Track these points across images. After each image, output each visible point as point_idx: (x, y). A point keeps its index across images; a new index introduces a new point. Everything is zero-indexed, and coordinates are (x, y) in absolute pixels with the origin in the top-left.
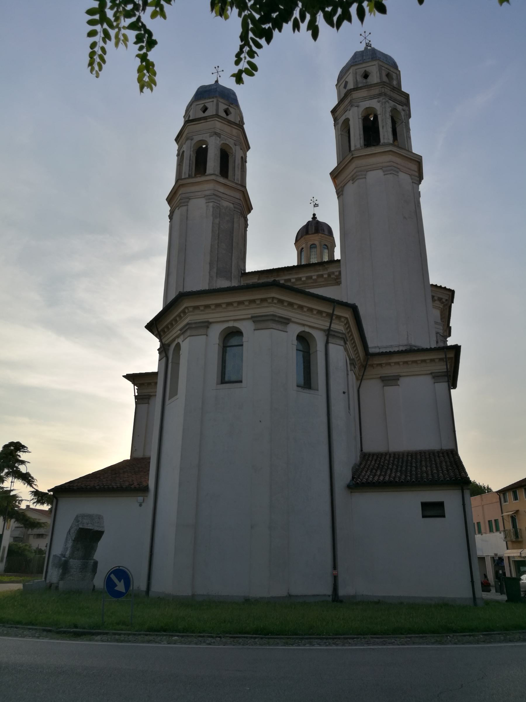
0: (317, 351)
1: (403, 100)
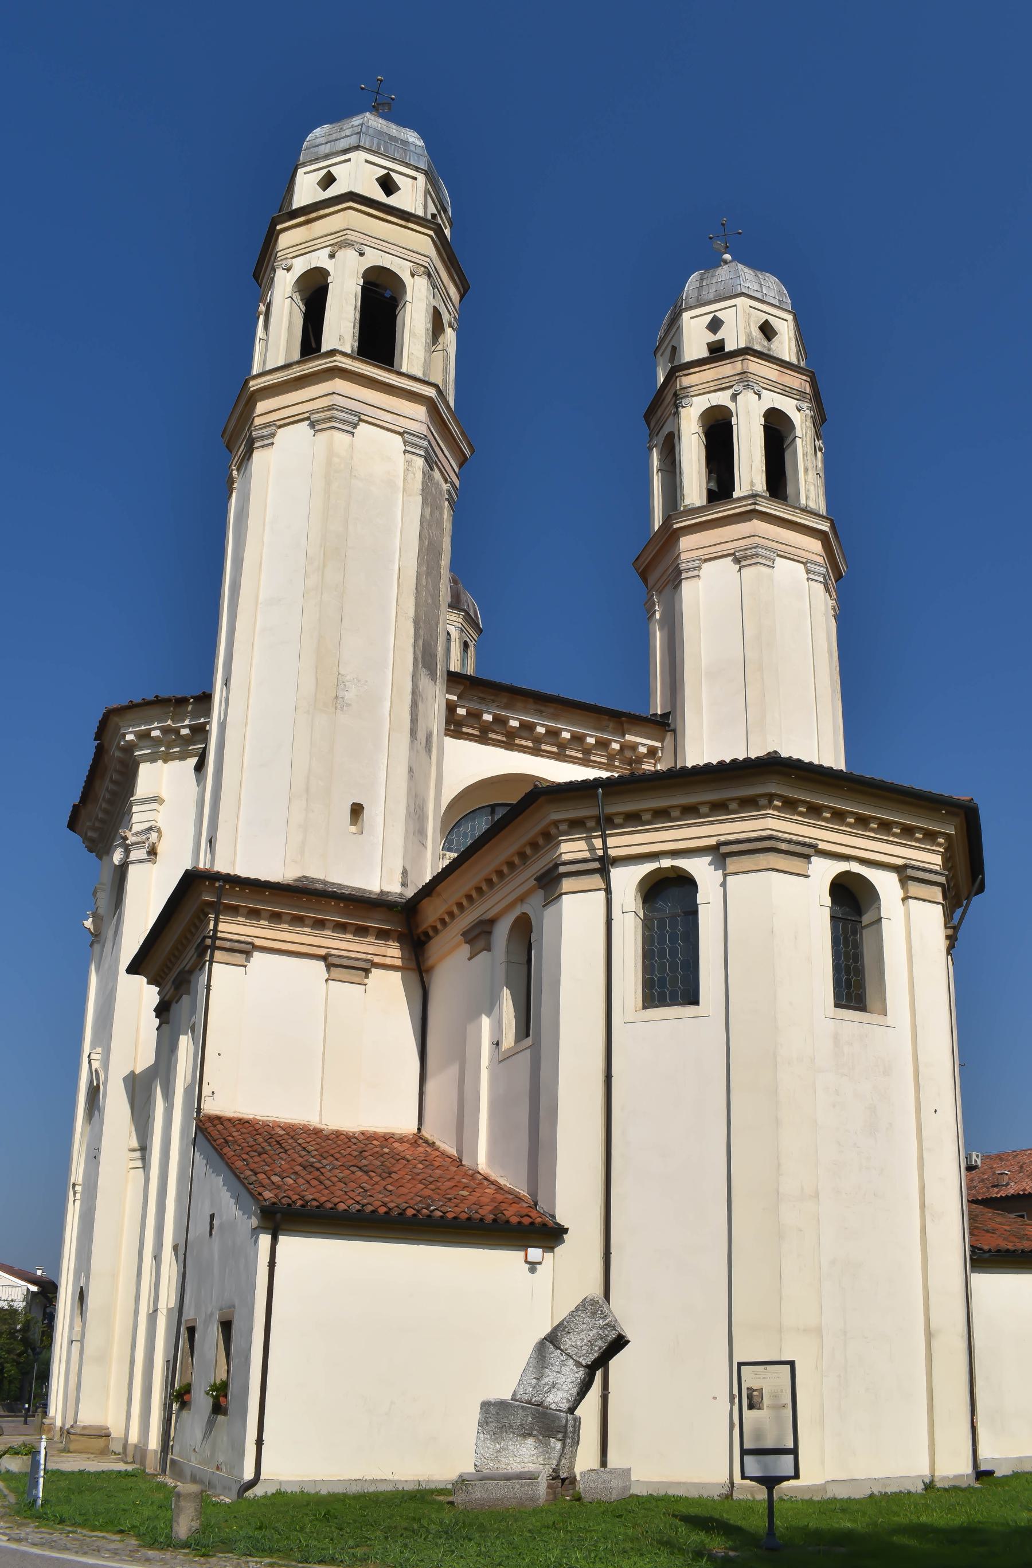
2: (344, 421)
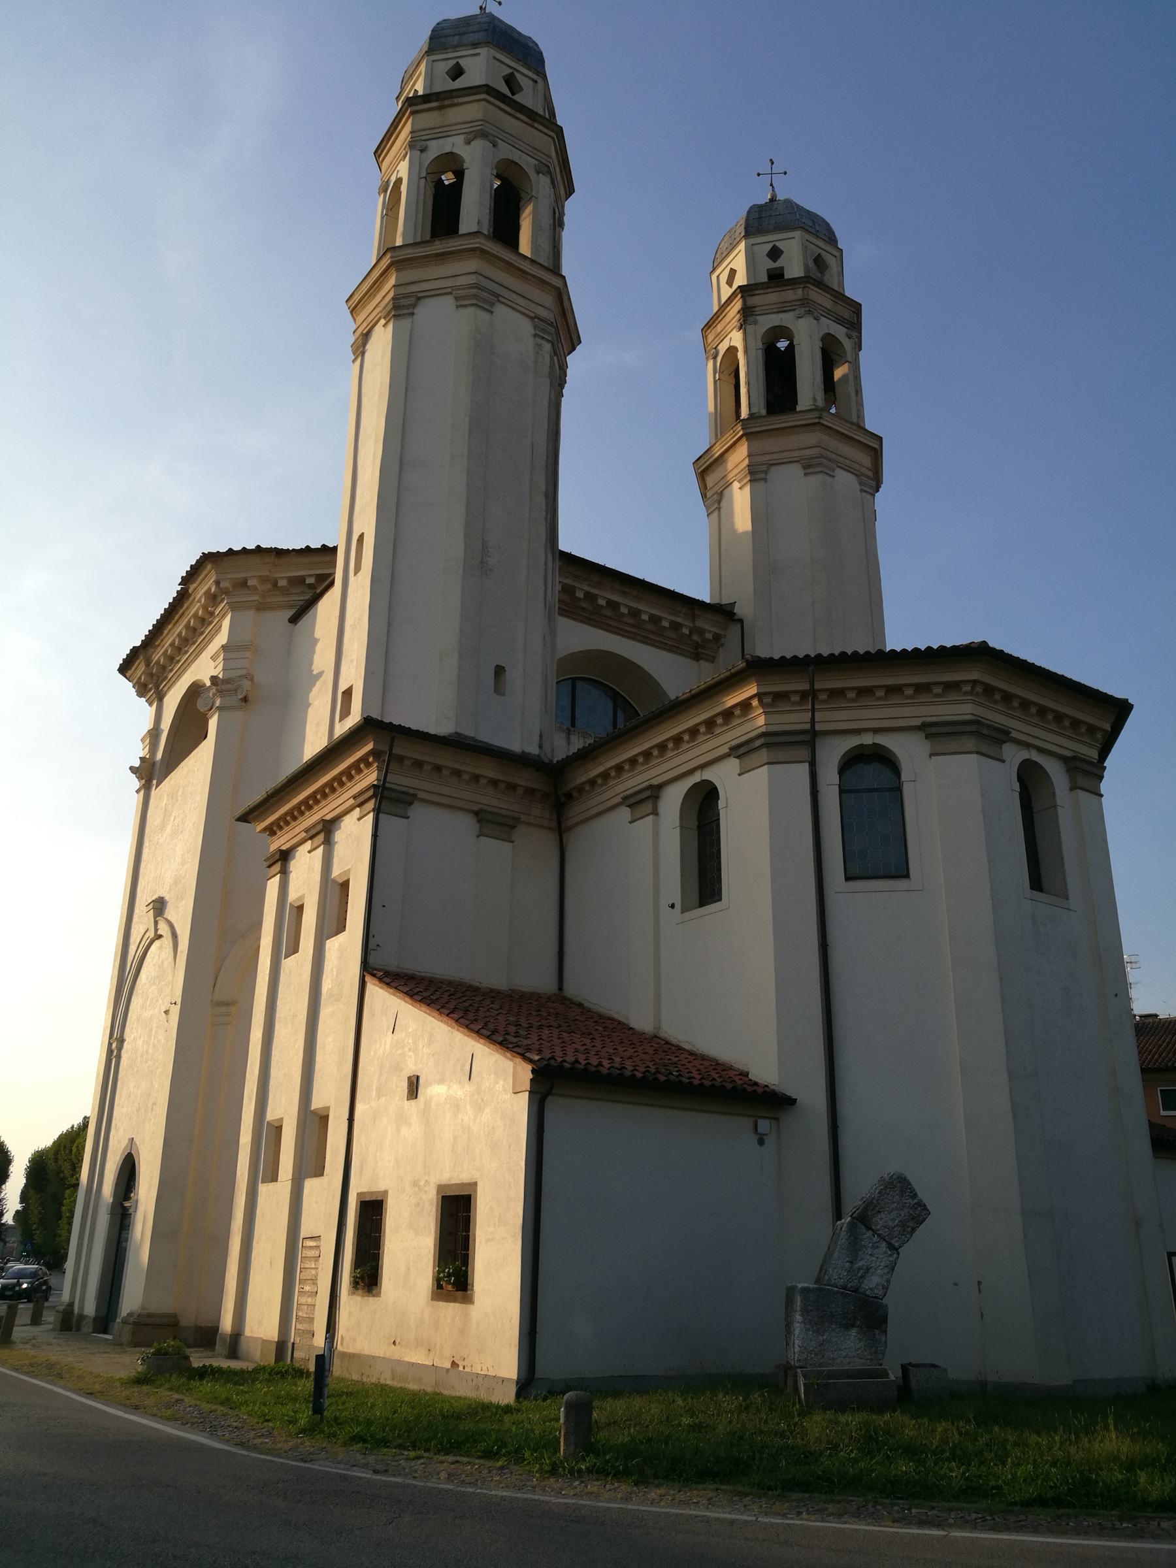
0: (1055, 806)
1: (846, 314)
2: (484, 301)
